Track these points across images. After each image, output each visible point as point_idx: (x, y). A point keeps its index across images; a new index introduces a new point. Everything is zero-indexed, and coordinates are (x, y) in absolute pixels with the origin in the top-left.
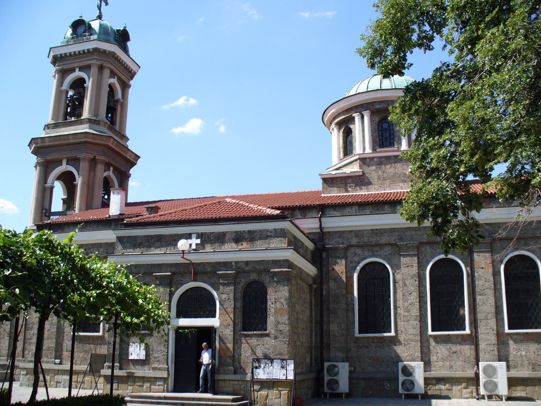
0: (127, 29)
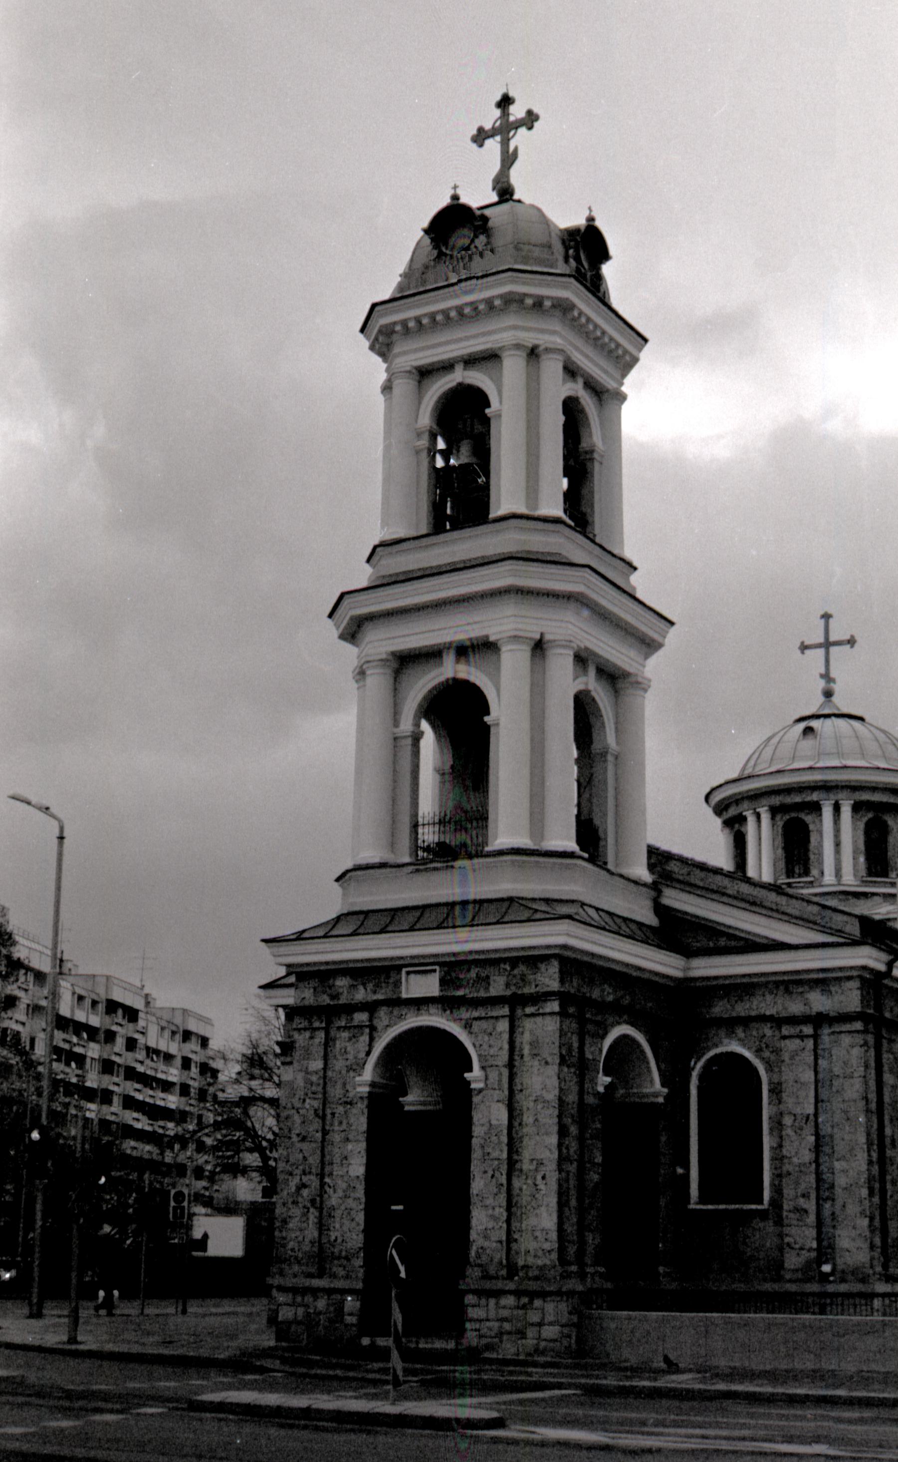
0: (599, 223)
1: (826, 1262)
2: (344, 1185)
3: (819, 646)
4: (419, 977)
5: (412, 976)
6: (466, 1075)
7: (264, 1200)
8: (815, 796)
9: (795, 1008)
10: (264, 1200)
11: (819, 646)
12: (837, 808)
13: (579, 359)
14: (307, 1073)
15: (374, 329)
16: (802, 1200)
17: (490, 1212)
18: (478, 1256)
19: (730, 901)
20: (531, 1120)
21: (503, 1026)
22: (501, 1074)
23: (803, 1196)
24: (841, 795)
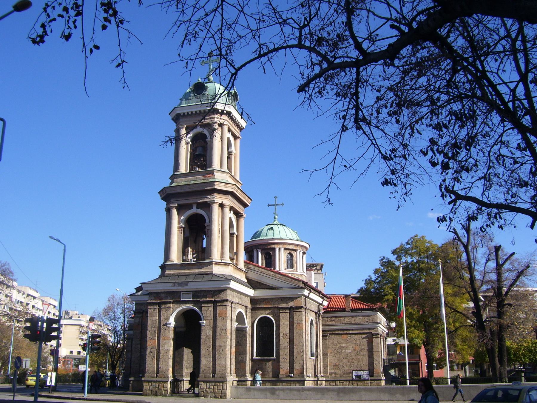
1: (141, 374)
2: (163, 352)
3: (274, 205)
4: (186, 295)
5: (184, 294)
6: (200, 322)
7: (257, 358)
8: (273, 246)
9: (284, 305)
10: (257, 358)
11: (274, 205)
12: (279, 249)
13: (231, 128)
14: (152, 320)
15: (174, 114)
16: (285, 356)
17: (207, 359)
18: (203, 371)
19: (267, 276)
20: (219, 334)
21: (211, 309)
22: (210, 322)
23: (285, 355)
24: (281, 246)
